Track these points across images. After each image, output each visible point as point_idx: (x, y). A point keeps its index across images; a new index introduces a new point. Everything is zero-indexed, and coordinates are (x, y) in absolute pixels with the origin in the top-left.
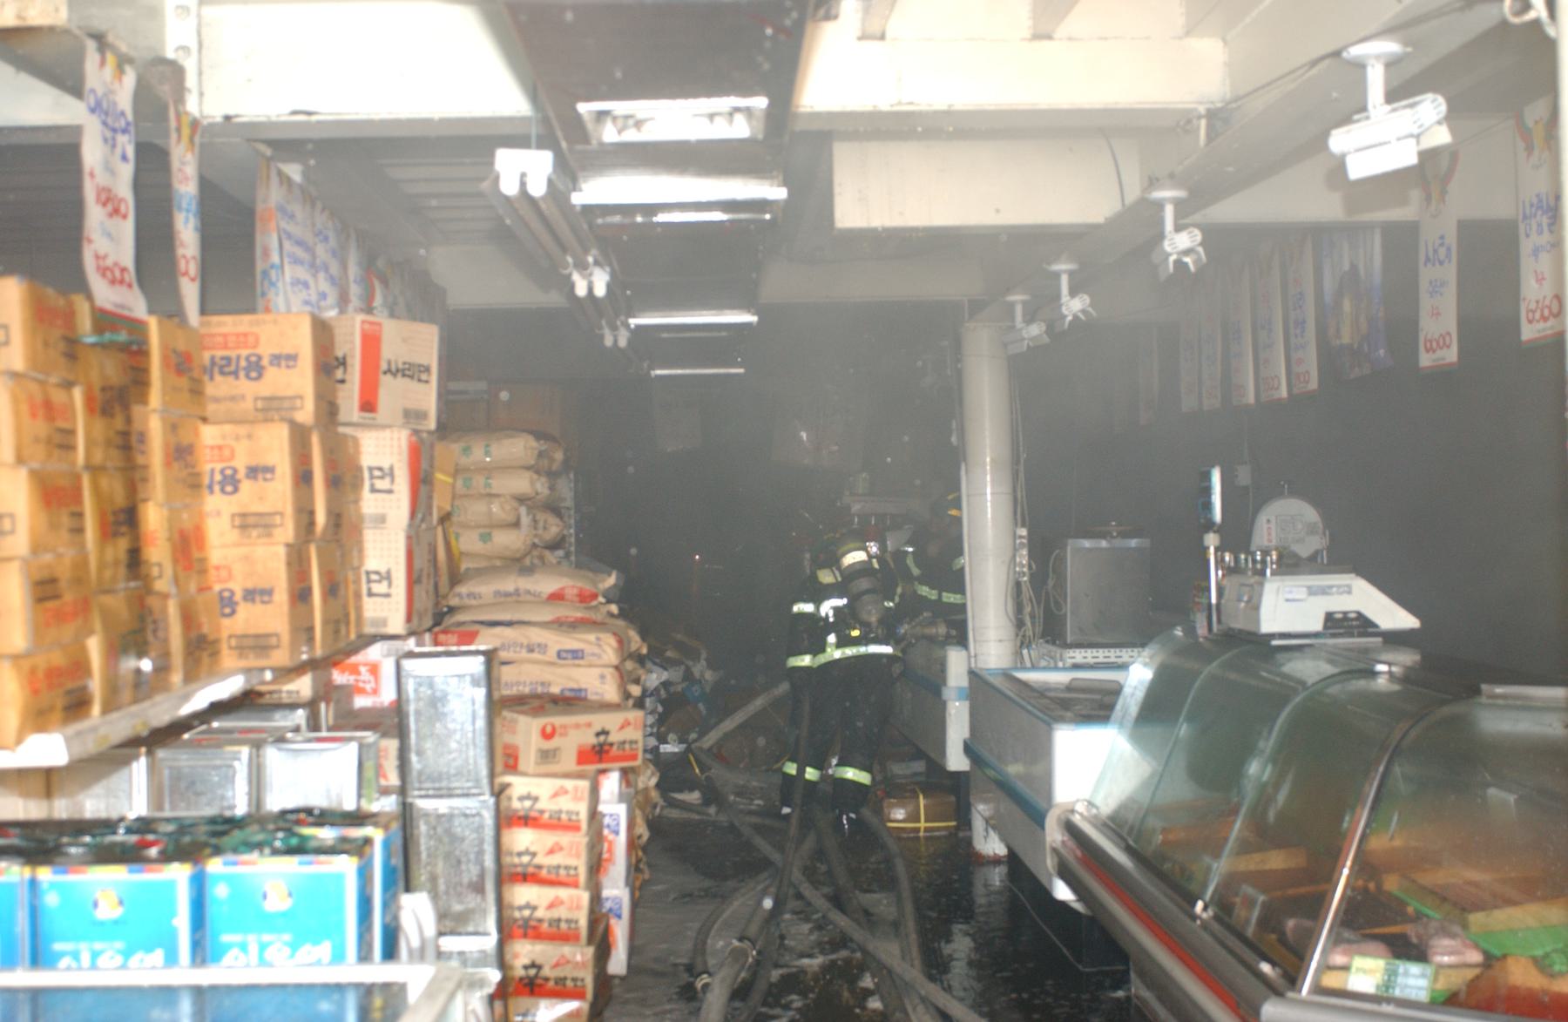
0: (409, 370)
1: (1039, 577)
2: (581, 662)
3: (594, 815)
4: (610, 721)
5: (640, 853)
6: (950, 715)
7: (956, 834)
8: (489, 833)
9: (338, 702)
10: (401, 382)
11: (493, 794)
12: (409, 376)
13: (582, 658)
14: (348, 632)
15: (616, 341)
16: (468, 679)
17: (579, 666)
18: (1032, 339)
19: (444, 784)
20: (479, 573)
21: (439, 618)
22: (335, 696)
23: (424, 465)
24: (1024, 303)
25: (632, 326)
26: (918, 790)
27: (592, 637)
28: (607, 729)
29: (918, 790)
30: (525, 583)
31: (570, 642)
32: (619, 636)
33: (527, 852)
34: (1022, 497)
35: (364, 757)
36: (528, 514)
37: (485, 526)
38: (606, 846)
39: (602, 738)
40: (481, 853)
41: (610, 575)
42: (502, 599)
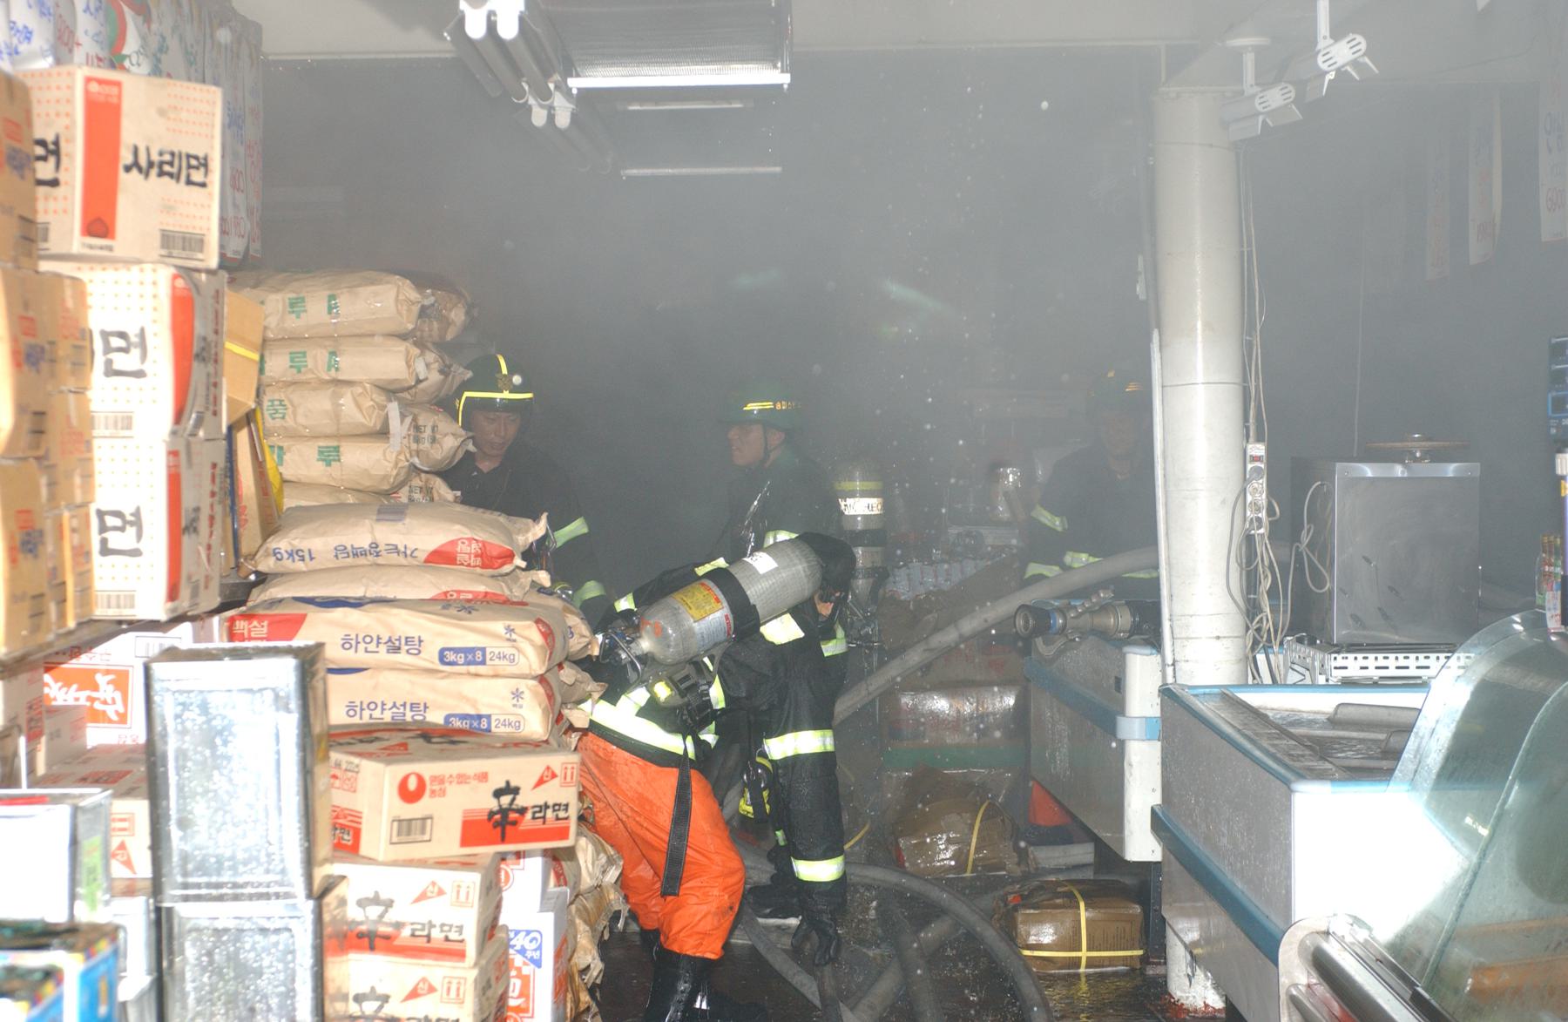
0: (171, 164)
1: (1286, 527)
2: (480, 669)
3: (490, 929)
4: (521, 770)
5: (585, 998)
6: (1130, 765)
7: (1142, 973)
8: (305, 959)
9: (54, 736)
10: (158, 186)
11: (310, 896)
12: (171, 175)
13: (483, 663)
14: (62, 615)
15: (551, 118)
16: (269, 695)
17: (477, 675)
18: (1270, 114)
19: (226, 877)
20: (305, 515)
21: (235, 598)
22: (48, 725)
23: (200, 328)
24: (1258, 50)
25: (575, 91)
26: (1076, 893)
27: (498, 627)
28: (513, 784)
29: (1076, 893)
30: (388, 534)
31: (462, 635)
32: (545, 624)
33: (373, 995)
34: (1257, 387)
35: (82, 830)
36: (403, 416)
37: (327, 437)
38: (515, 985)
39: (505, 800)
40: (290, 994)
41: (536, 519)
42: (350, 561)
